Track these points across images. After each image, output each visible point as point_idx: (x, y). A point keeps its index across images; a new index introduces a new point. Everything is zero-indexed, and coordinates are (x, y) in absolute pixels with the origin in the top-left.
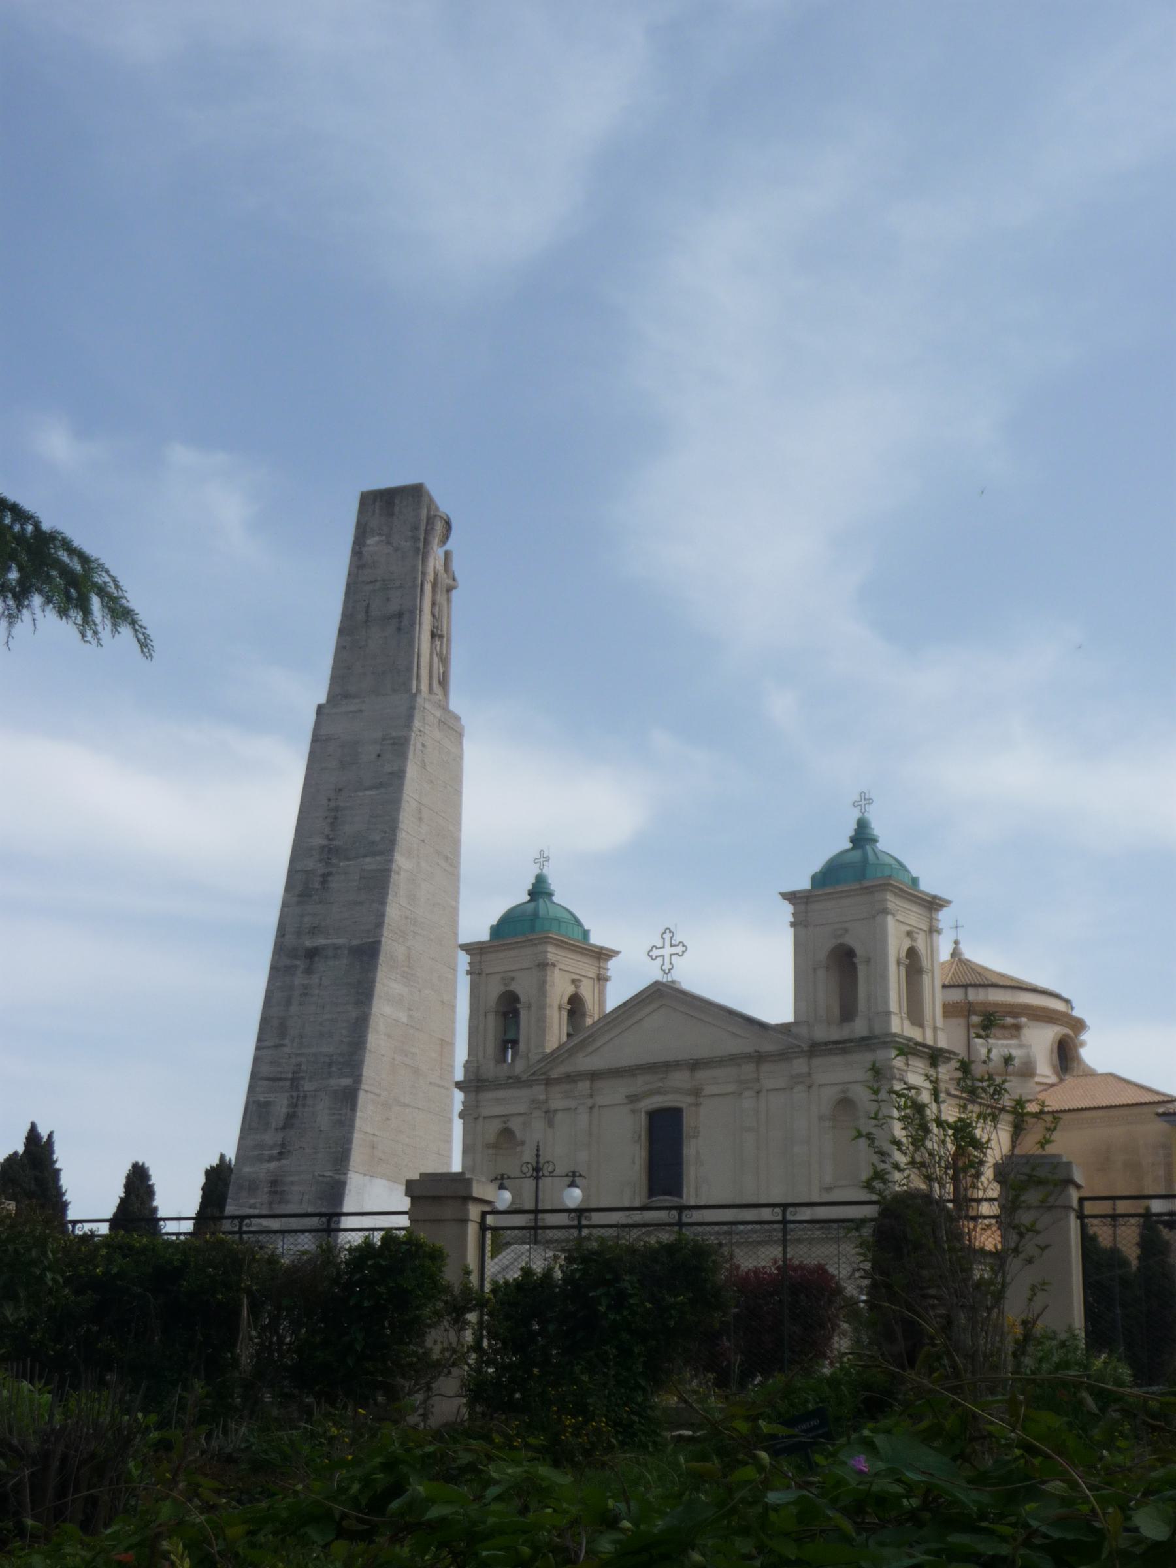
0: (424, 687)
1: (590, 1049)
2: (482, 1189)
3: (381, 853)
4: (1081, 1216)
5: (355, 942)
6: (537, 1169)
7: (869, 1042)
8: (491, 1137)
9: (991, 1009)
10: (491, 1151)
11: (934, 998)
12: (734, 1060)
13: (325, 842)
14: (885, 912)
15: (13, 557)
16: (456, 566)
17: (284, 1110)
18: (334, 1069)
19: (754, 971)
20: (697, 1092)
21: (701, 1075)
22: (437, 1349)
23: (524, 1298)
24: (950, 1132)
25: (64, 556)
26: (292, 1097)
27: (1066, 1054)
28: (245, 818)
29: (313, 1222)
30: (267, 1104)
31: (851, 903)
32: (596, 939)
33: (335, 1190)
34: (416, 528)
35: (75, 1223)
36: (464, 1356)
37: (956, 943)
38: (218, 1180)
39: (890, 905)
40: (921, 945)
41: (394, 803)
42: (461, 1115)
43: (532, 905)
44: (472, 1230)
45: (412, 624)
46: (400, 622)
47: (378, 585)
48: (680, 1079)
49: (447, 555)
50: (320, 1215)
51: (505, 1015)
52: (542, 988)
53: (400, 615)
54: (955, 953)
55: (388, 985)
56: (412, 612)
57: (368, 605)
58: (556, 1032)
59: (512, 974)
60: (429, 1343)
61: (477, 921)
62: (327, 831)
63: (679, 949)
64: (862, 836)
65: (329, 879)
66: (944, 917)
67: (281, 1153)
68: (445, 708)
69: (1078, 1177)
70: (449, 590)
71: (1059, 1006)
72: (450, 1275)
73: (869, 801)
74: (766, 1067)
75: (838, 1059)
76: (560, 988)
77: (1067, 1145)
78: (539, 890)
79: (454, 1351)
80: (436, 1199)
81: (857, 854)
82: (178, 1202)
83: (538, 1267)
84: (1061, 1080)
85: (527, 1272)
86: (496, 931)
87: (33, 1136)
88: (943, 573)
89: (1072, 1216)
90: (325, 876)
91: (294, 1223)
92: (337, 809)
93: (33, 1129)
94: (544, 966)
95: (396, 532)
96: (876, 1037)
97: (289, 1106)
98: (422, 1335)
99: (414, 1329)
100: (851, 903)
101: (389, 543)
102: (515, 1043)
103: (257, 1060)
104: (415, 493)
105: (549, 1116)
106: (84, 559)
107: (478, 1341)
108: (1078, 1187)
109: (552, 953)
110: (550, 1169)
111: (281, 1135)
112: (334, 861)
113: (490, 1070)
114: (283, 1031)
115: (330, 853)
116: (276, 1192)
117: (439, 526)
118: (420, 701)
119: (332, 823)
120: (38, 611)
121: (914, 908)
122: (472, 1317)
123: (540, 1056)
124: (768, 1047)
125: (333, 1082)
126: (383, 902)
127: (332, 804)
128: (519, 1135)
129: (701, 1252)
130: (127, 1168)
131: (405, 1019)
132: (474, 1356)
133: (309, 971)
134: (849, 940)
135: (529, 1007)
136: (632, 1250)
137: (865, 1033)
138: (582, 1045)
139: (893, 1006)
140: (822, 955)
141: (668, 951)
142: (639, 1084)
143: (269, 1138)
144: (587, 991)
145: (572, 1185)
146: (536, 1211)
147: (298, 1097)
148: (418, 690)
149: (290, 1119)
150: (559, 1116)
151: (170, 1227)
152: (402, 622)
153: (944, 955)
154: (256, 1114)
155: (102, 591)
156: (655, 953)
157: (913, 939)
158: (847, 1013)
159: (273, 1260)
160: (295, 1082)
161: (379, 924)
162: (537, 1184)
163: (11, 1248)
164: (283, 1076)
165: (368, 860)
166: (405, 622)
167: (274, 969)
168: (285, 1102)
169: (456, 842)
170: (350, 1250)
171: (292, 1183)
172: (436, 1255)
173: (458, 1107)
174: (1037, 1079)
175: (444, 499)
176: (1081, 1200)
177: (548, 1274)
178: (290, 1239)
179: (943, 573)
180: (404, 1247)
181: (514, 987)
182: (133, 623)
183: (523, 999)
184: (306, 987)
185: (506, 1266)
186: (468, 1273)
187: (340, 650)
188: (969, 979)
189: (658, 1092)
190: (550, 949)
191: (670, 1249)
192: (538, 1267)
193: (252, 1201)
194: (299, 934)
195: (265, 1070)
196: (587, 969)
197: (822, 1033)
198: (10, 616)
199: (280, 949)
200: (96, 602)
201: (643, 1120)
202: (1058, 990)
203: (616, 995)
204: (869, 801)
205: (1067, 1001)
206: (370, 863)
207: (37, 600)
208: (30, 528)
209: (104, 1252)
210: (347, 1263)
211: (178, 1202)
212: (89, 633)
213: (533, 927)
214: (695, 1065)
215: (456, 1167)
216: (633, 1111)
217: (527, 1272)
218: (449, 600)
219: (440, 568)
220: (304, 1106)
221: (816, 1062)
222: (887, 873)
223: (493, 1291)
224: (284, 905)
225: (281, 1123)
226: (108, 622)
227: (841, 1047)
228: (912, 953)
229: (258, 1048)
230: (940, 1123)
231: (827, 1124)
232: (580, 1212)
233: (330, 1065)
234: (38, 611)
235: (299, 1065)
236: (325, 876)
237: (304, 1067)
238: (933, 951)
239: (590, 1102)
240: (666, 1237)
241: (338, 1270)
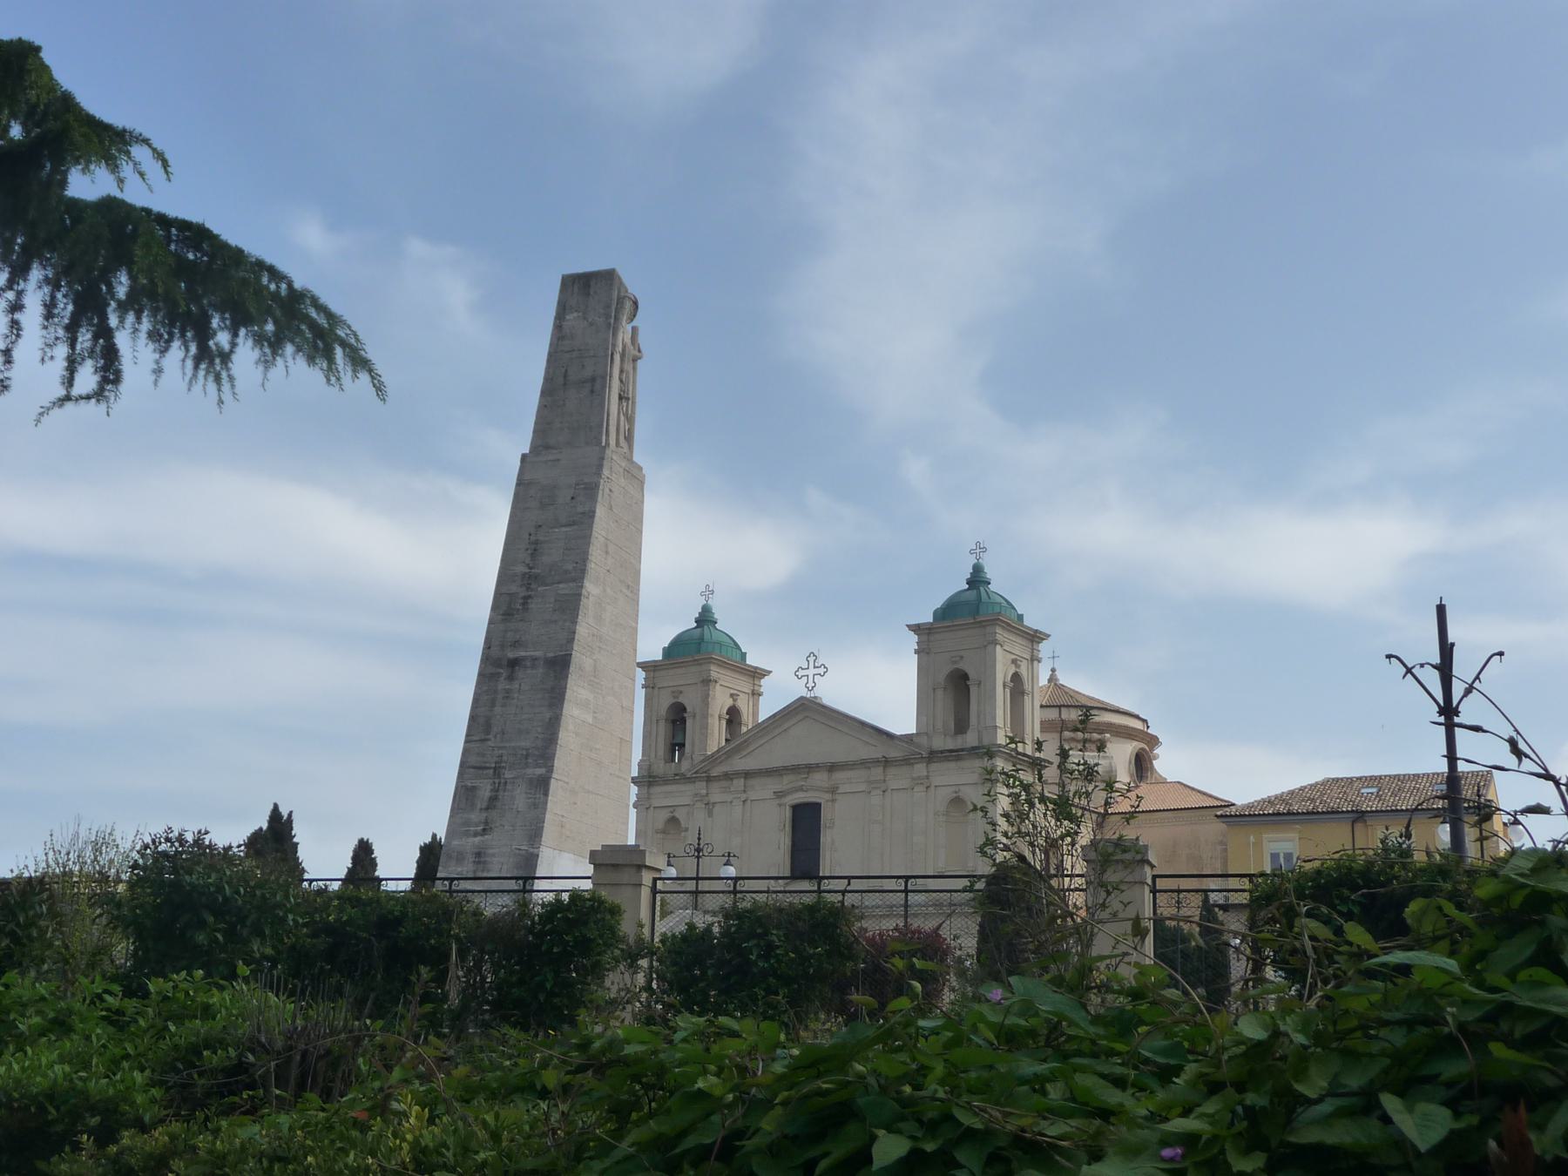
0: (612, 442)
2: (655, 859)
3: (574, 580)
4: (1154, 891)
5: (550, 655)
6: (698, 850)
8: (660, 825)
9: (1084, 722)
11: (1034, 719)
12: (864, 764)
14: (995, 642)
15: (269, 312)
16: (641, 339)
17: (488, 794)
19: (882, 688)
20: (833, 790)
21: (839, 776)
22: (614, 989)
23: (689, 948)
24: (1051, 806)
25: (313, 313)
27: (1142, 765)
28: (459, 554)
29: (512, 885)
30: (474, 788)
31: (967, 632)
33: (531, 860)
34: (608, 306)
35: (311, 881)
36: (636, 996)
37: (1053, 670)
38: (430, 855)
39: (999, 637)
40: (1024, 671)
41: (586, 538)
42: (635, 806)
44: (645, 893)
45: (604, 387)
47: (575, 354)
48: (819, 778)
49: (634, 329)
50: (517, 878)
51: (674, 722)
53: (593, 380)
54: (1052, 678)
55: (577, 690)
56: (604, 378)
58: (717, 736)
60: (607, 983)
61: (652, 644)
63: (822, 670)
64: (977, 579)
66: (1044, 648)
68: (630, 460)
69: (1152, 857)
70: (635, 360)
71: (1138, 725)
72: (626, 927)
73: (984, 550)
74: (892, 771)
75: (952, 765)
76: (720, 701)
77: (1144, 834)
78: (705, 618)
79: (628, 991)
80: (615, 866)
82: (397, 868)
83: (701, 925)
85: (691, 926)
86: (668, 652)
87: (275, 814)
88: (1052, 361)
89: (1147, 889)
90: (526, 598)
91: (494, 885)
92: (536, 542)
93: (276, 807)
94: (707, 682)
95: (591, 308)
98: (602, 978)
99: (597, 971)
100: (967, 632)
102: (682, 746)
103: (466, 752)
104: (609, 277)
105: (710, 806)
106: (330, 315)
107: (649, 982)
108: (1153, 867)
109: (715, 672)
113: (661, 768)
114: (488, 727)
115: (530, 579)
117: (628, 305)
118: (608, 452)
120: (290, 359)
121: (1019, 640)
122: (644, 963)
124: (894, 753)
125: (529, 771)
126: (575, 622)
129: (839, 914)
130: (352, 844)
131: (590, 720)
132: (645, 995)
133: (511, 678)
134: (965, 666)
136: (781, 910)
138: (737, 750)
139: (1000, 723)
140: (941, 677)
141: (811, 671)
142: (786, 782)
143: (475, 816)
144: (743, 704)
146: (697, 879)
148: (608, 444)
149: (493, 800)
151: (391, 886)
152: (595, 386)
153: (1043, 680)
154: (464, 795)
155: (344, 344)
156: (800, 673)
157: (1018, 666)
158: (961, 726)
159: (477, 913)
160: (497, 771)
161: (571, 640)
163: (258, 893)
166: (598, 386)
167: (481, 675)
168: (489, 787)
169: (637, 574)
170: (543, 905)
172: (615, 911)
173: (633, 798)
175: (632, 282)
176: (1154, 877)
177: (708, 929)
178: (491, 898)
179: (1052, 361)
180: (588, 904)
182: (370, 371)
184: (508, 691)
185: (672, 924)
186: (642, 926)
187: (543, 408)
188: (1061, 699)
189: (801, 789)
191: (812, 909)
192: (701, 925)
194: (502, 646)
195: (473, 760)
196: (743, 685)
197: (939, 743)
198: (266, 361)
199: (487, 659)
200: (339, 351)
201: (788, 813)
202: (1136, 712)
203: (768, 707)
204: (984, 550)
205: (1145, 721)
206: (564, 588)
207: (289, 349)
208: (284, 286)
209: (336, 903)
210: (540, 916)
211: (397, 868)
212: (333, 379)
213: (700, 649)
214: (832, 768)
215: (631, 841)
217: (691, 926)
218: (634, 369)
219: (628, 340)
221: (934, 766)
222: (997, 609)
223: (661, 941)
224: (490, 622)
225: (485, 805)
226: (349, 369)
227: (955, 755)
228: (1016, 677)
229: (466, 742)
230: (1043, 799)
232: (736, 879)
233: (527, 756)
234: (290, 359)
236: (526, 598)
238: (1034, 678)
239: (744, 797)
240: (808, 899)
241: (533, 922)
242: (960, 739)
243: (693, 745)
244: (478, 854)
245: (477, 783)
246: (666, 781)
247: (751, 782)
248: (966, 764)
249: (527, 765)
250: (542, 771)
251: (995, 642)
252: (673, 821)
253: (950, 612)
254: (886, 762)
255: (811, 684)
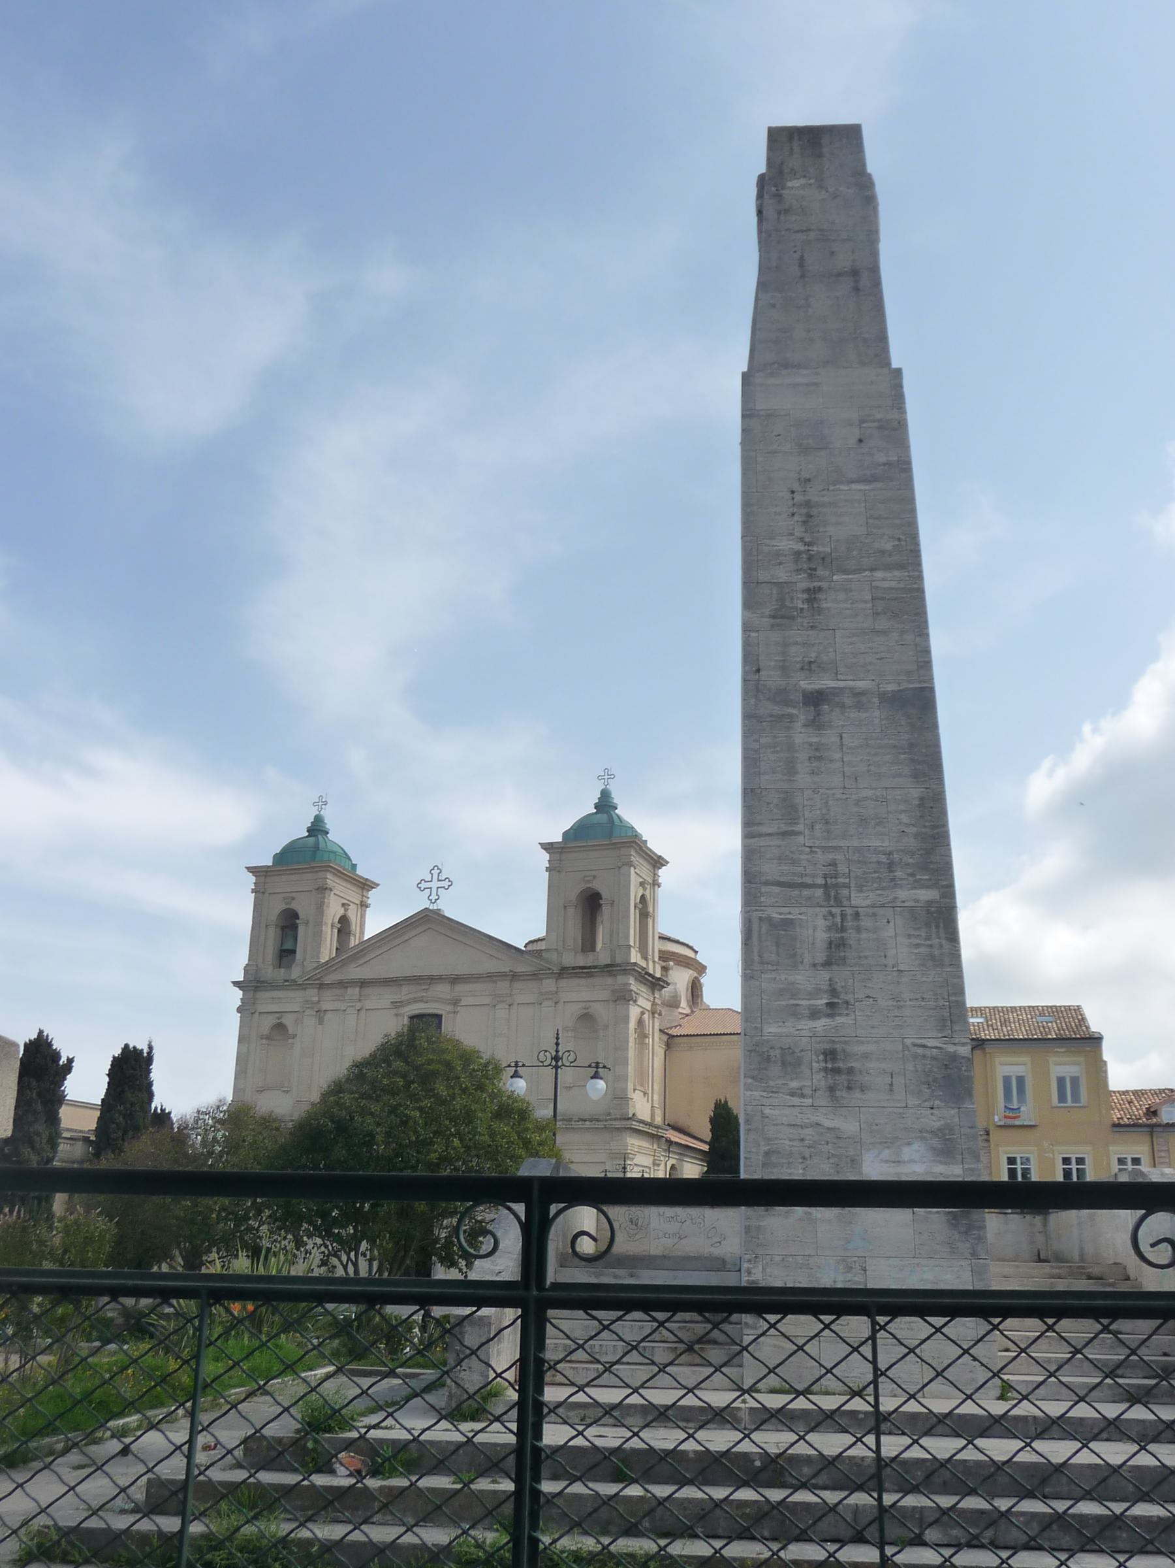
1: (361, 962)
5: (891, 687)
6: (556, 1058)
7: (611, 969)
8: (265, 1031)
10: (264, 1041)
12: (490, 977)
13: (800, 547)
14: (630, 864)
17: (822, 936)
18: (899, 874)
20: (456, 1003)
21: (461, 988)
26: (833, 915)
27: (695, 989)
30: (788, 923)
32: (361, 872)
40: (647, 893)
43: (312, 839)
46: (857, 281)
47: (812, 235)
51: (283, 928)
52: (320, 908)
53: (855, 273)
57: (802, 257)
58: (328, 950)
59: (294, 895)
62: (799, 531)
63: (446, 884)
65: (821, 596)
67: (831, 1005)
71: (691, 954)
74: (518, 985)
75: (583, 981)
81: (603, 818)
84: (692, 1012)
94: (323, 889)
96: (618, 965)
97: (829, 929)
101: (821, 187)
105: (320, 1014)
109: (331, 880)
110: (572, 1058)
111: (824, 975)
112: (821, 572)
113: (269, 972)
114: (790, 811)
116: (837, 1071)
119: (805, 522)
123: (315, 965)
124: (521, 968)
127: (799, 498)
128: (291, 1031)
135: (307, 923)
137: (608, 962)
138: (345, 963)
140: (573, 895)
142: (405, 993)
145: (596, 1076)
147: (843, 916)
149: (836, 951)
150: (329, 1016)
156: (423, 885)
158: (589, 945)
160: (832, 891)
162: (556, 1074)
164: (809, 881)
165: (879, 574)
166: (865, 281)
168: (821, 923)
171: (866, 1056)
174: (680, 1010)
181: (294, 906)
183: (301, 915)
189: (421, 1000)
190: (329, 876)
193: (794, 1084)
196: (353, 895)
197: (569, 960)
214: (455, 980)
216: (396, 1015)
220: (858, 930)
221: (563, 983)
225: (821, 957)
227: (586, 972)
231: (570, 1034)
233: (891, 866)
235: (834, 864)
237: (842, 868)
242: (591, 956)
243: (305, 952)
244: (830, 1055)
245: (794, 913)
246: (273, 986)
247: (366, 991)
248: (596, 981)
249: (895, 883)
250: (927, 895)
251: (630, 864)
252: (280, 1027)
253: (580, 833)
254: (514, 977)
255: (434, 897)
